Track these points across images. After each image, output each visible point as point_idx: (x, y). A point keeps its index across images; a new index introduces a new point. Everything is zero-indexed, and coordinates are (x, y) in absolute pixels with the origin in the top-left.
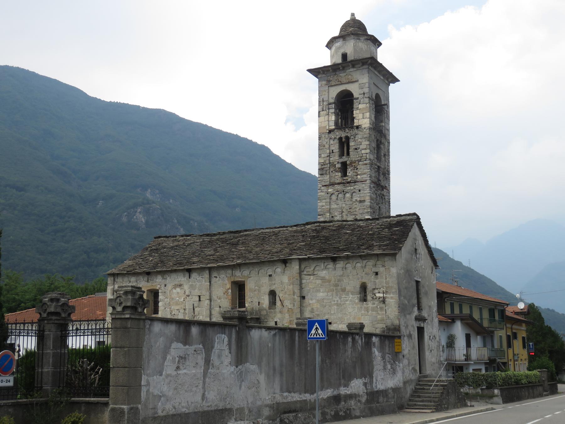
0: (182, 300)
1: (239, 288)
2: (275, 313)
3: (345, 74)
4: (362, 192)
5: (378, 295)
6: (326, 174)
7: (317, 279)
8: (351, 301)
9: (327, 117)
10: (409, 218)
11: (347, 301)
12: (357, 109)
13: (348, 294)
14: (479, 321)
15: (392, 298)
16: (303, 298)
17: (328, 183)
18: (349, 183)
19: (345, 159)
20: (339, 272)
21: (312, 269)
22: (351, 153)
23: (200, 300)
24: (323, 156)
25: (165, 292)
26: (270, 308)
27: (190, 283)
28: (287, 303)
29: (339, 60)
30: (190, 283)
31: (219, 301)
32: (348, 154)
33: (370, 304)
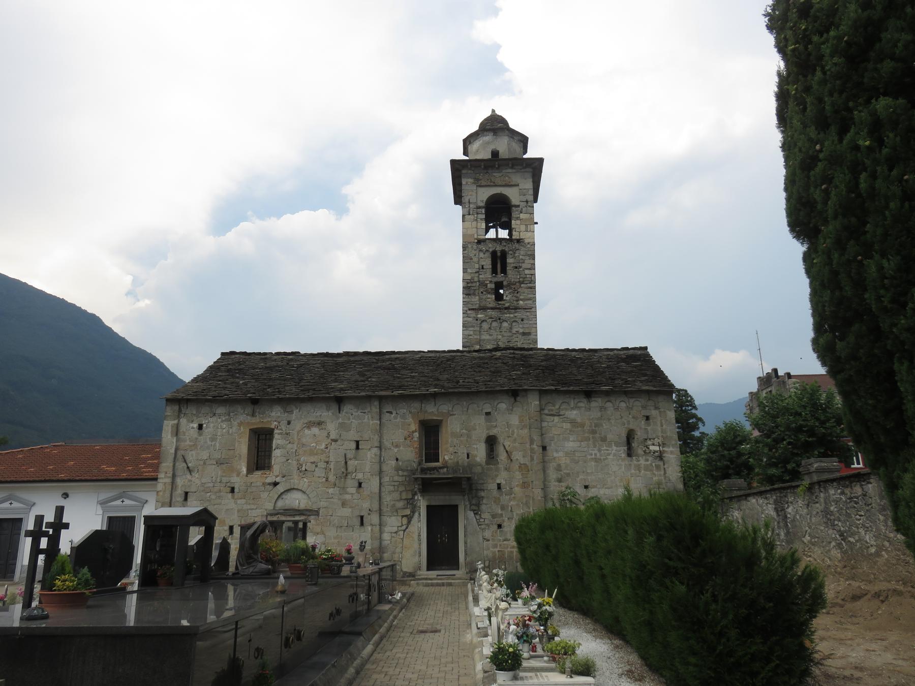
0: (323, 446)
1: (430, 432)
2: (498, 470)
4: (525, 322)
5: (652, 448)
6: (474, 294)
7: (563, 422)
8: (615, 455)
9: (475, 223)
10: (639, 352)
11: (609, 454)
12: (518, 218)
13: (610, 445)
15: (672, 453)
16: (544, 448)
17: (477, 307)
19: (500, 277)
20: (595, 414)
21: (557, 407)
23: (357, 448)
24: (469, 271)
26: (487, 463)
28: (518, 456)
29: (488, 156)
31: (396, 450)
32: (504, 271)
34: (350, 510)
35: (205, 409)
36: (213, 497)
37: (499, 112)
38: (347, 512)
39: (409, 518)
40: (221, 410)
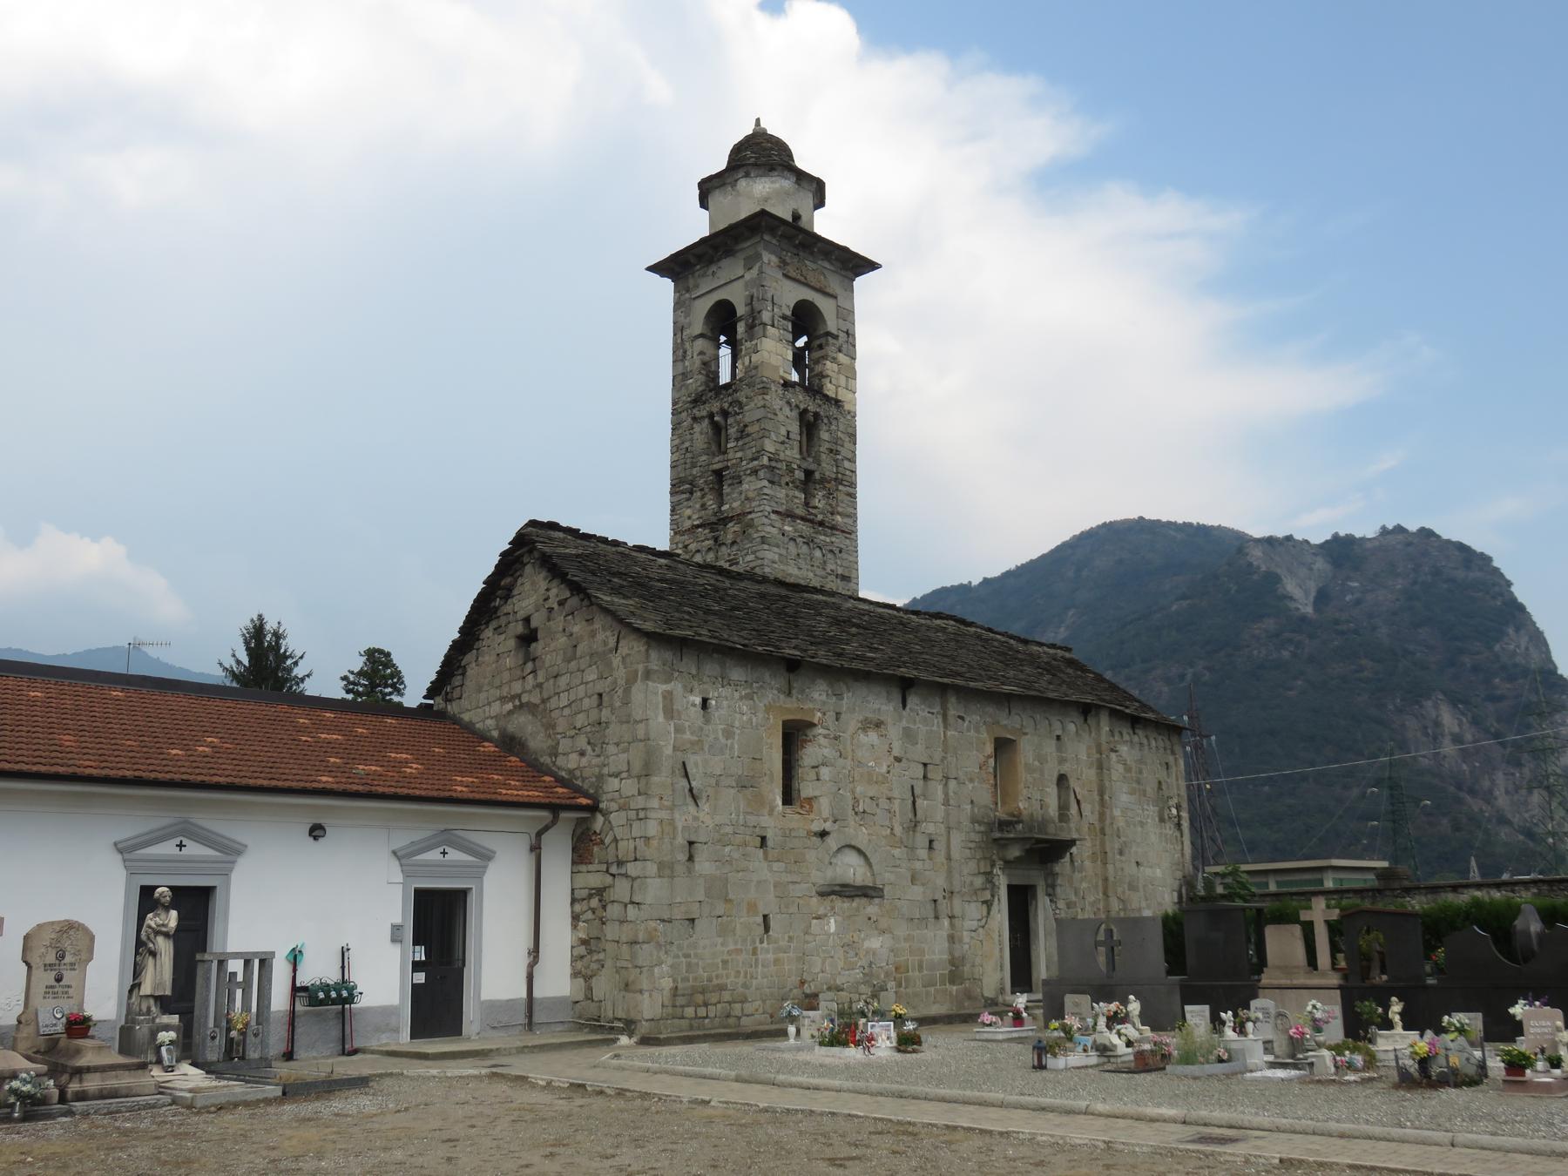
0: (884, 769)
3: (814, 266)
4: (844, 555)
12: (834, 360)
25: (836, 738)
27: (904, 723)
30: (904, 723)
34: (921, 889)
35: (711, 668)
36: (736, 855)
37: (773, 129)
38: (917, 892)
39: (988, 904)
40: (737, 674)
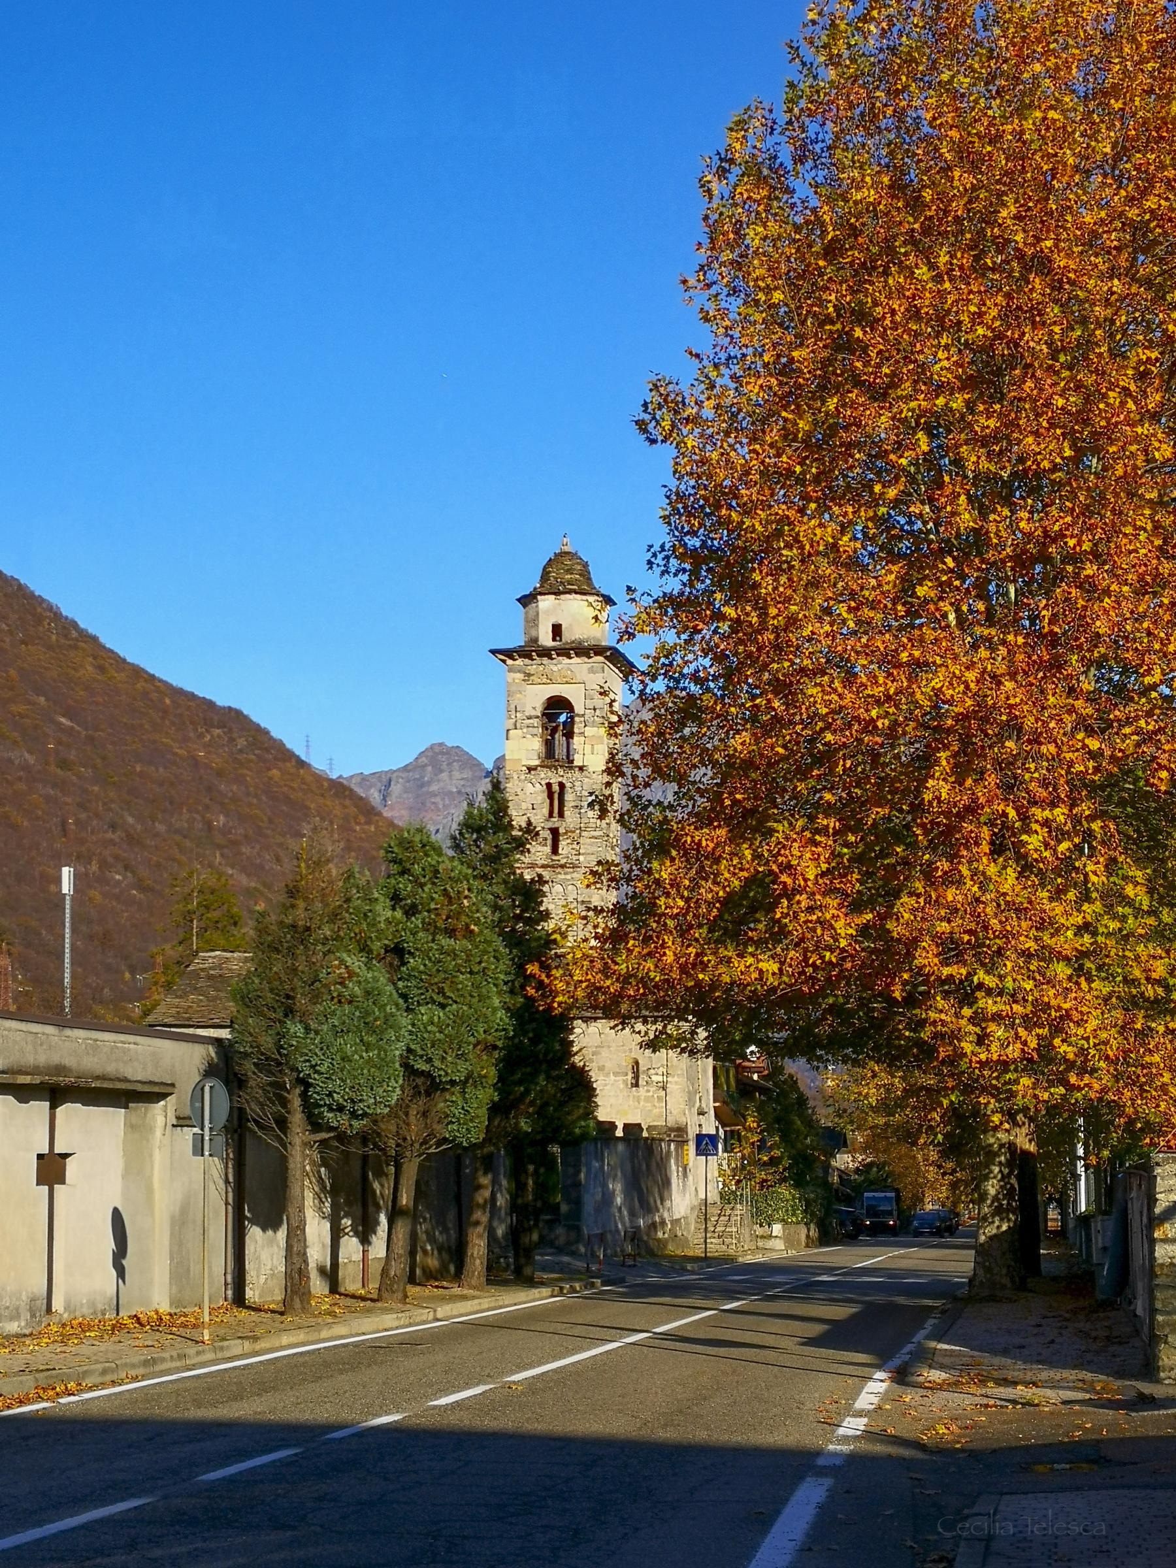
14: (1157, 1210)
18: (562, 866)
22: (567, 814)
32: (561, 815)
33: (642, 1091)
